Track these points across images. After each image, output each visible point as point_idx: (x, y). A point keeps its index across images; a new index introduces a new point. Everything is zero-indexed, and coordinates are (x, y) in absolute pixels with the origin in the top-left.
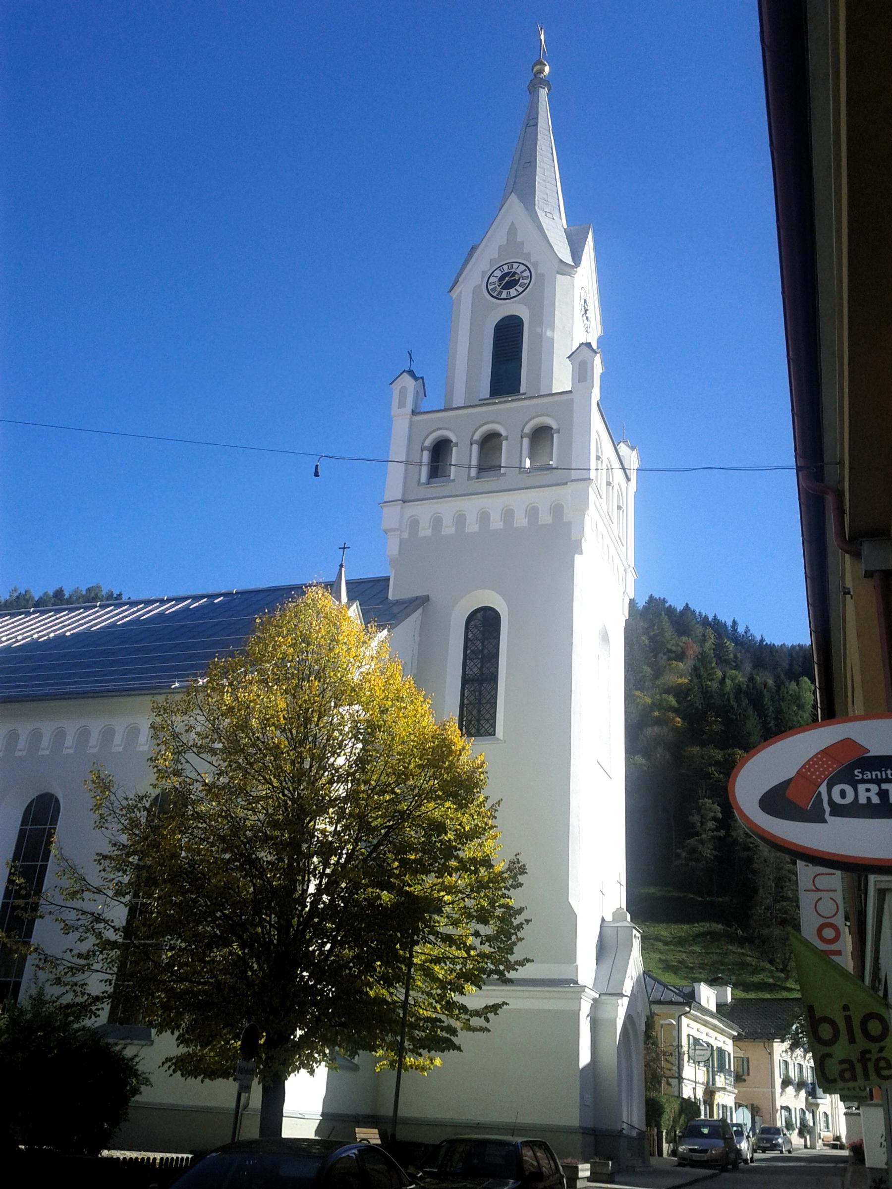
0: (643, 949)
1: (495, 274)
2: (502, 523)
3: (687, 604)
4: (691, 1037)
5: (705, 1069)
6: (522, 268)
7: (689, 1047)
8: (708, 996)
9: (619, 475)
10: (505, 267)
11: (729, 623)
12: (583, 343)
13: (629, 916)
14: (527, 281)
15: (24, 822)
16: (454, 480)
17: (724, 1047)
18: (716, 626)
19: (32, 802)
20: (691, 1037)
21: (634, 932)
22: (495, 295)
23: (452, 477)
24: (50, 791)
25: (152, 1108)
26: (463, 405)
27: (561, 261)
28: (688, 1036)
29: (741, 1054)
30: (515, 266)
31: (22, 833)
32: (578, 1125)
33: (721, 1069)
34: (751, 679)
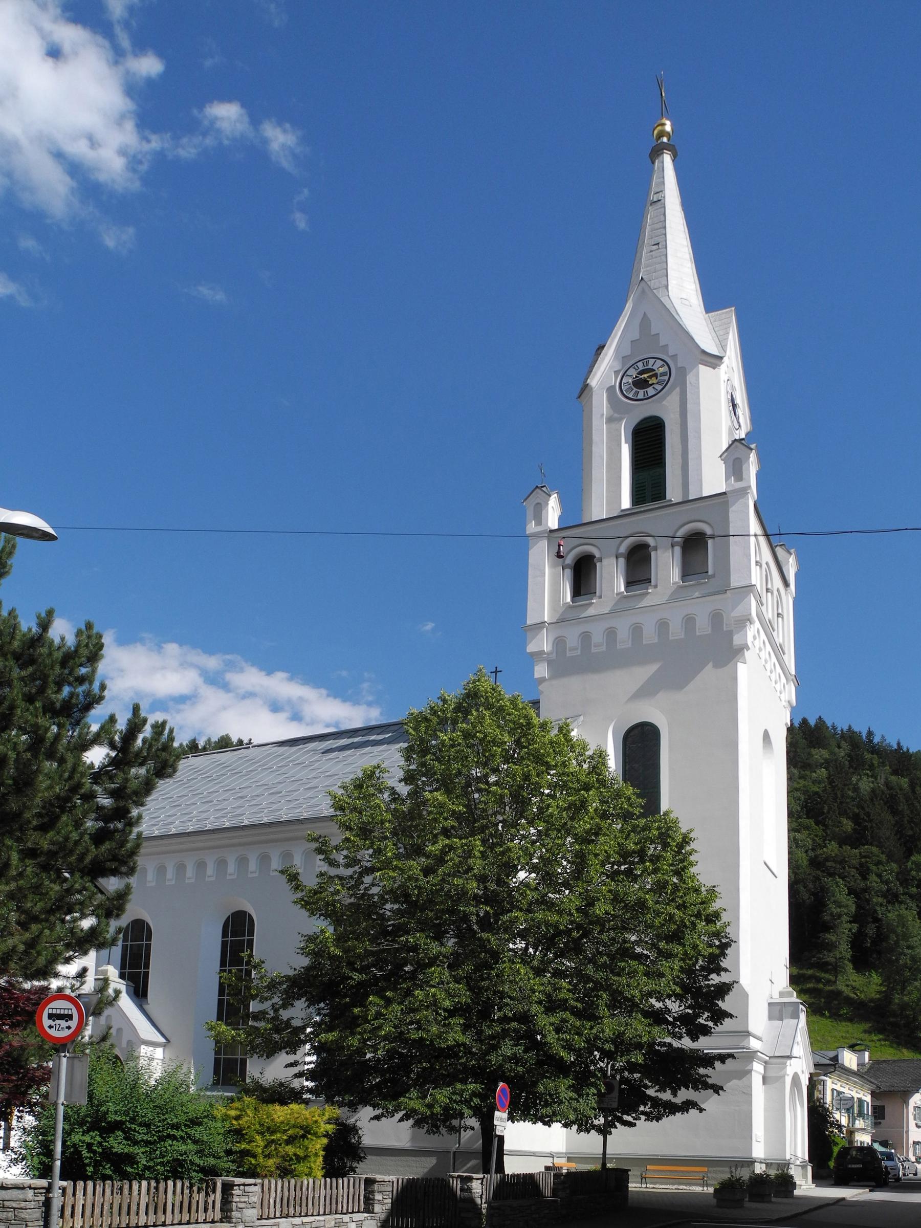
0: (808, 1023)
1: (628, 373)
2: (710, 629)
3: (820, 717)
4: (835, 1092)
5: (846, 1115)
6: (660, 363)
7: (833, 1099)
8: (849, 1059)
9: (777, 582)
10: (640, 365)
11: (864, 735)
12: (736, 440)
13: (795, 993)
14: (666, 378)
15: (225, 934)
16: (713, 576)
17: (864, 1098)
18: (851, 737)
19: (228, 918)
20: (835, 1092)
21: (801, 1006)
22: (630, 396)
23: (710, 573)
24: (241, 909)
25: (765, 1153)
26: (680, 500)
27: (704, 352)
28: (833, 1090)
29: (878, 1103)
30: (651, 361)
31: (224, 944)
32: (564, 1151)
33: (861, 1114)
34: (887, 784)
